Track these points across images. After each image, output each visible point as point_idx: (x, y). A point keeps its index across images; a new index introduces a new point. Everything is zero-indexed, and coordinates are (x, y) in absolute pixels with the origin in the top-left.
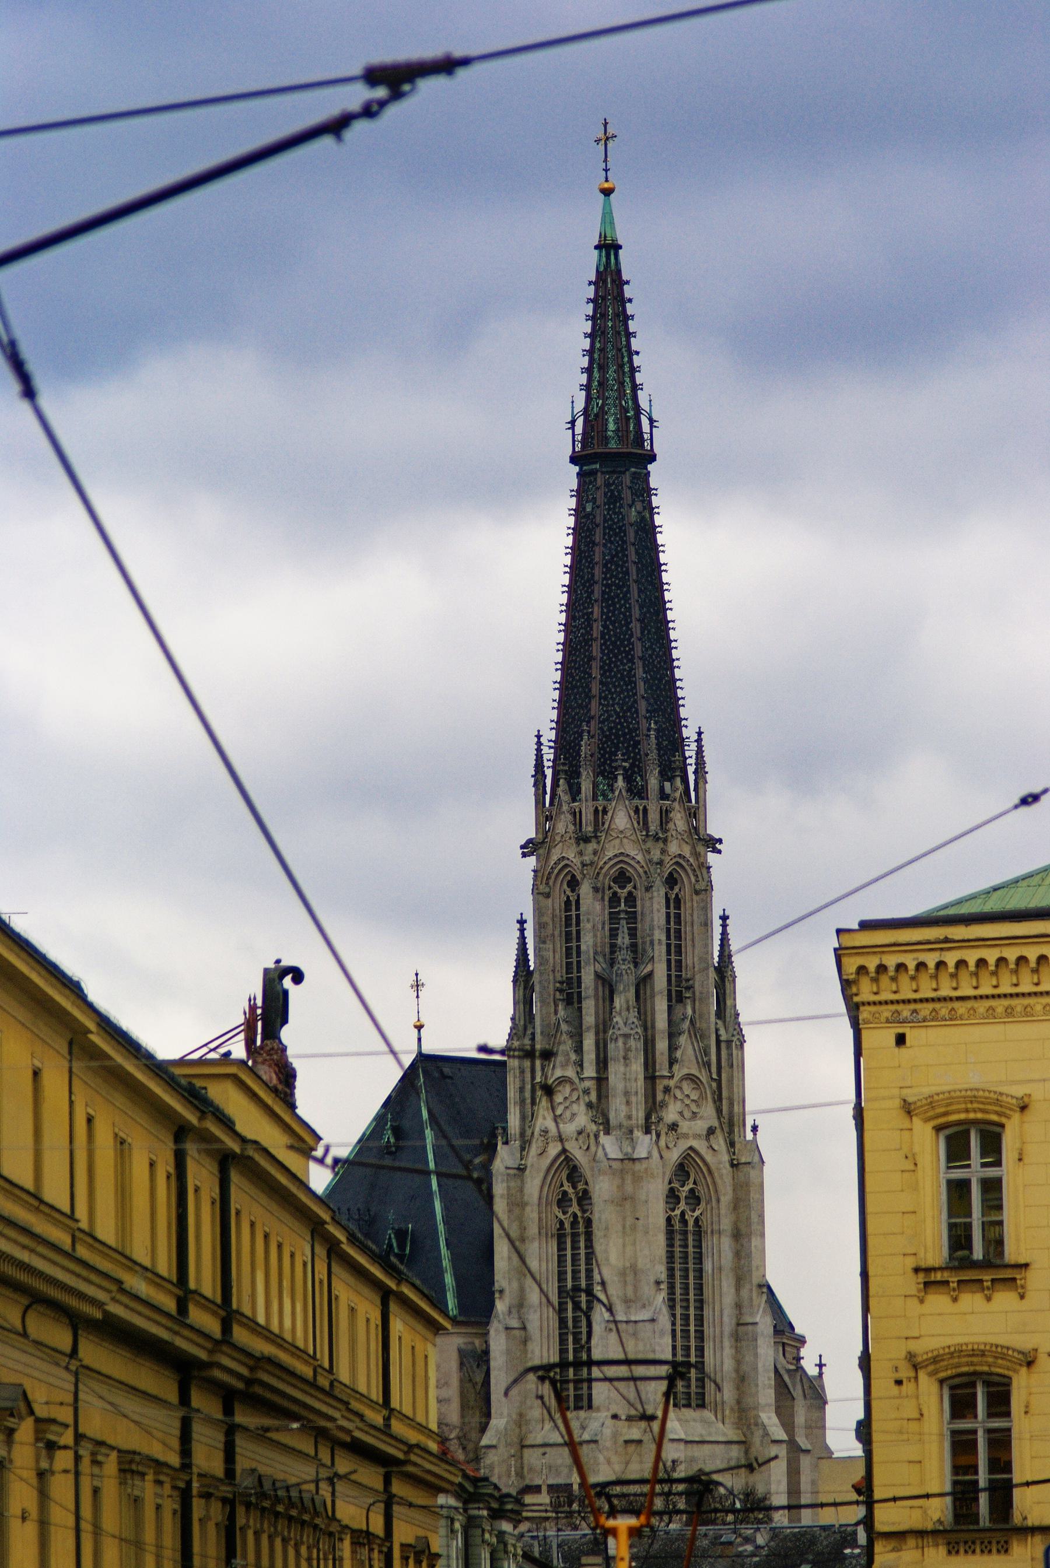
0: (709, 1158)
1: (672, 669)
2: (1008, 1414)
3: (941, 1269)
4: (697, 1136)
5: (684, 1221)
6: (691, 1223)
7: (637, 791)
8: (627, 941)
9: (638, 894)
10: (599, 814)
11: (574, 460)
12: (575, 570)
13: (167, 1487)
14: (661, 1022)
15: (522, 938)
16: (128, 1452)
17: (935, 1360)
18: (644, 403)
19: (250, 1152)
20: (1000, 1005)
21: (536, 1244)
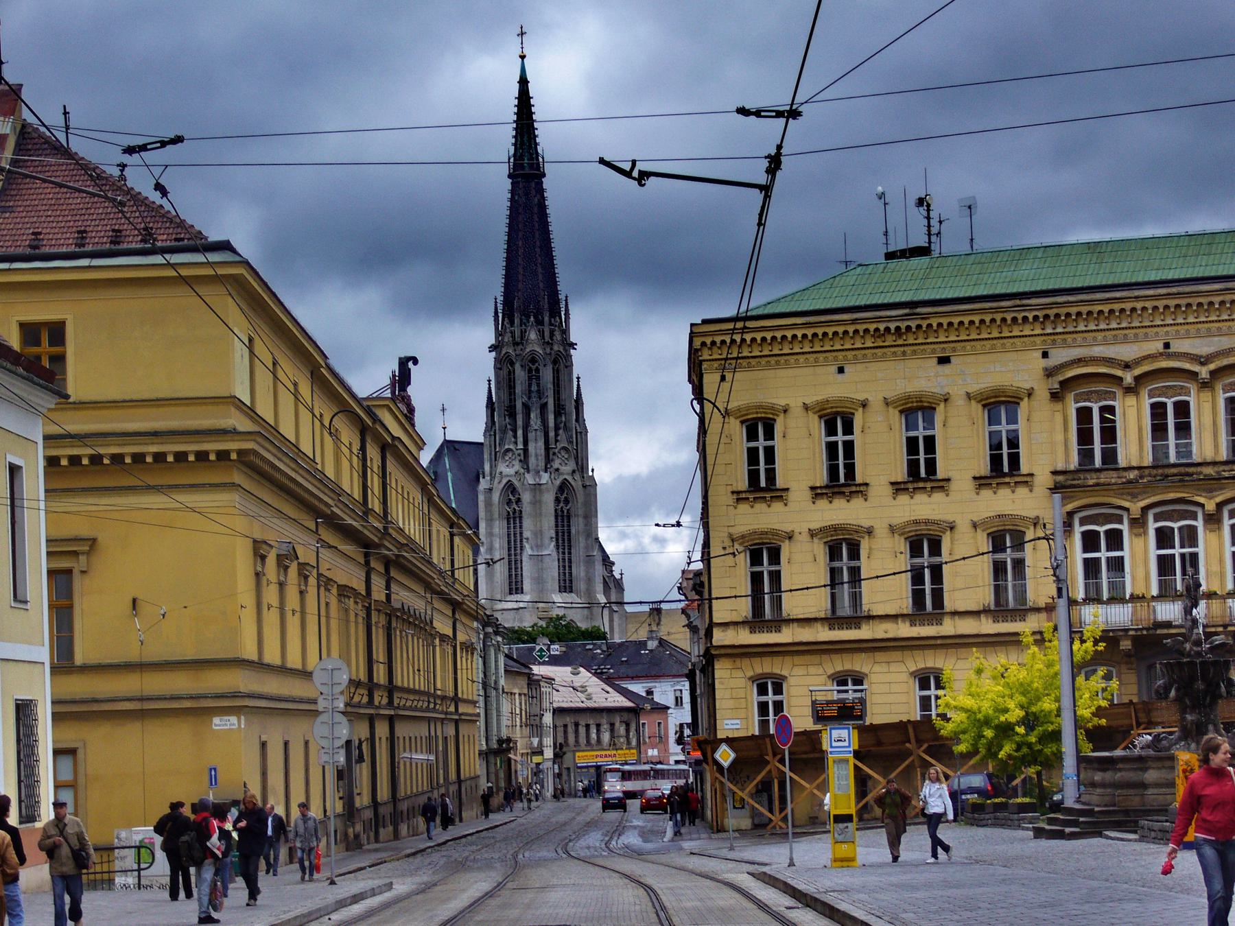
0: (573, 483)
1: (554, 268)
2: (779, 563)
3: (745, 492)
4: (568, 474)
5: (562, 511)
6: (565, 512)
7: (540, 322)
8: (536, 388)
9: (540, 367)
10: (523, 333)
11: (510, 176)
12: (510, 226)
13: (360, 605)
14: (551, 423)
15: (490, 388)
16: (342, 586)
17: (743, 537)
18: (540, 151)
19: (397, 443)
20: (773, 360)
21: (498, 522)
